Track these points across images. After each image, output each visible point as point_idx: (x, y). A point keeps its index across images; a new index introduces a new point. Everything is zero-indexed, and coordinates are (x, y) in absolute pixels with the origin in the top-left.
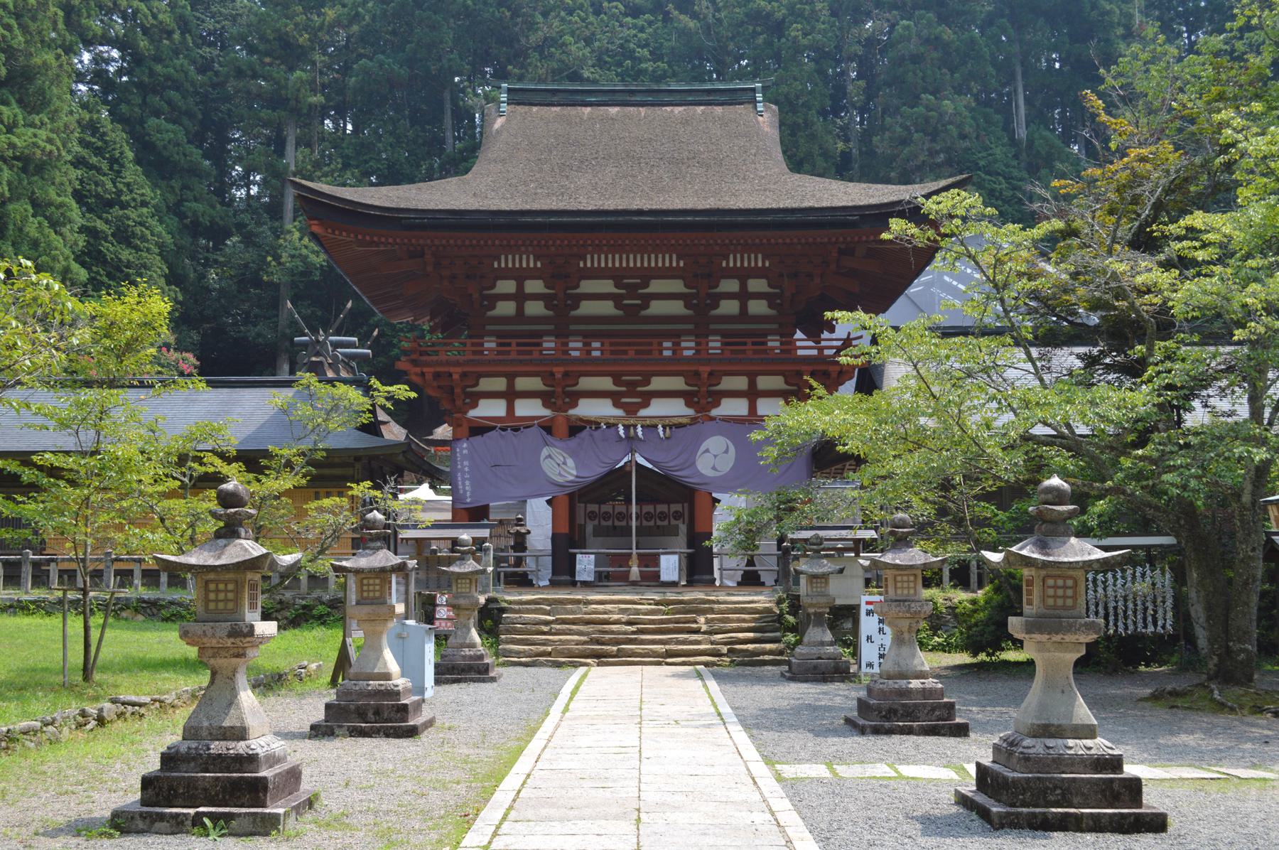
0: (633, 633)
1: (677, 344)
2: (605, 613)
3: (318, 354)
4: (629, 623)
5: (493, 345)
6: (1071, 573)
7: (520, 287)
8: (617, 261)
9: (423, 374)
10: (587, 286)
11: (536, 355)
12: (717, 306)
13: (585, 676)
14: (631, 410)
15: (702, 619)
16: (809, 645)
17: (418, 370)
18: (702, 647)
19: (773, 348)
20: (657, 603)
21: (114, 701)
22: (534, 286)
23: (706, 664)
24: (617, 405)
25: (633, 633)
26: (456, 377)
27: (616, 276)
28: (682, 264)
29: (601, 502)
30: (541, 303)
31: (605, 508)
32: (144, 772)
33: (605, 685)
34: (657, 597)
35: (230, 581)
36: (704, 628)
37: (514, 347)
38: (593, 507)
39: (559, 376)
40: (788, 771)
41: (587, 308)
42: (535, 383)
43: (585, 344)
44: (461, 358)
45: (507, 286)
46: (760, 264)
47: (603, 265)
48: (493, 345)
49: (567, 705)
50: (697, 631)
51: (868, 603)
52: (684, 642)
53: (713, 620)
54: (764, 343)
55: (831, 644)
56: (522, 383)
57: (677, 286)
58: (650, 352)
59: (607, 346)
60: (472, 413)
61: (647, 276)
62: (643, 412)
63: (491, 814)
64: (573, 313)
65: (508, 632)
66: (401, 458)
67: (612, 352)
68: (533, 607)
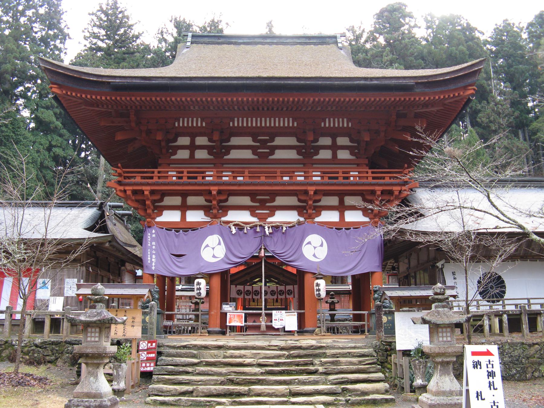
0: (262, 374)
2: (240, 357)
4: (260, 365)
8: (253, 122)
9: (125, 191)
10: (235, 141)
11: (200, 179)
12: (317, 154)
14: (263, 218)
15: (317, 361)
16: (438, 393)
17: (122, 188)
20: (282, 349)
22: (201, 141)
24: (253, 214)
25: (262, 374)
26: (146, 193)
27: (253, 133)
28: (295, 125)
29: (244, 284)
30: (206, 151)
31: (248, 288)
34: (282, 344)
36: (321, 369)
38: (240, 287)
39: (214, 193)
41: (234, 154)
42: (200, 200)
46: (345, 125)
47: (245, 125)
51: (474, 354)
52: (304, 383)
53: (326, 363)
56: (191, 200)
57: (292, 141)
60: (158, 219)
62: (270, 220)
66: (107, 245)
68: (183, 351)
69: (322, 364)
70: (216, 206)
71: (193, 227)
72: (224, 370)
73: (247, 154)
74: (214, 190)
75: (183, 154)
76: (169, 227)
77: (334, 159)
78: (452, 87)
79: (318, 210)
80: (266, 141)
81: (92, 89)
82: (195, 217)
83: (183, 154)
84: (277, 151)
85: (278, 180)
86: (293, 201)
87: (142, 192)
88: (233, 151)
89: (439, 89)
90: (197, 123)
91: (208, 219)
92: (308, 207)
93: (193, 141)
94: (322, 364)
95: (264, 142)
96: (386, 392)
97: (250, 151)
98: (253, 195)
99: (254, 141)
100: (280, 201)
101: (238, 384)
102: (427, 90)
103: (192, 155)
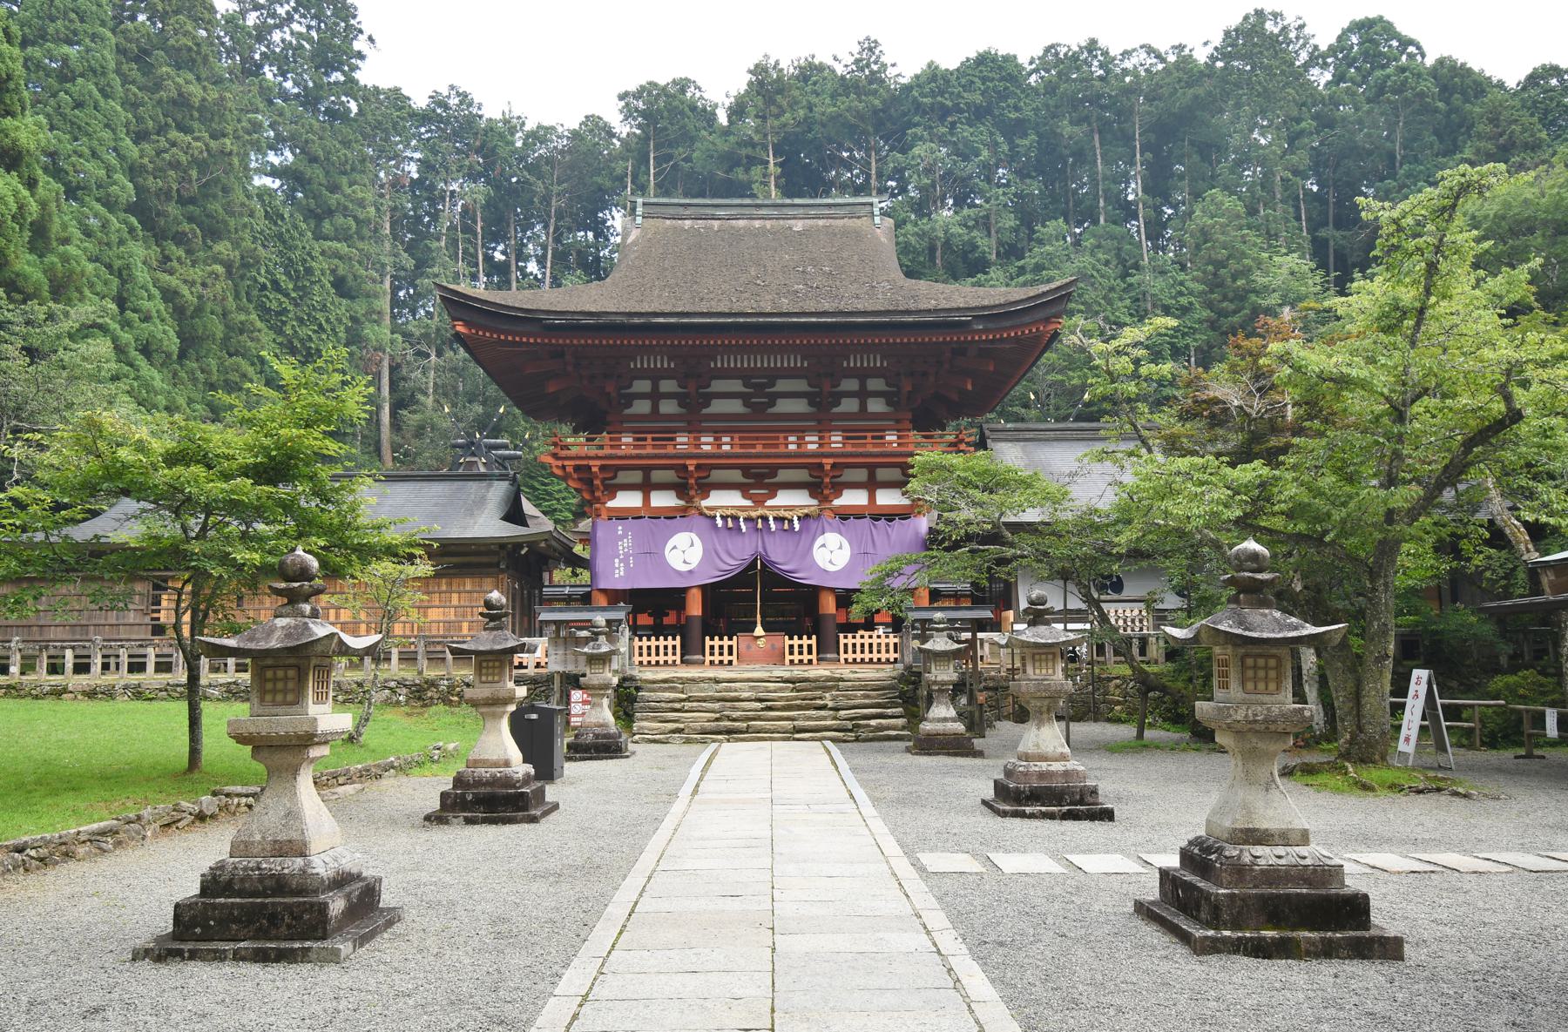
1: (801, 438)
3: (473, 454)
4: (761, 700)
5: (630, 440)
6: (1274, 651)
7: (655, 386)
9: (564, 467)
10: (718, 386)
13: (714, 754)
17: (560, 463)
18: (829, 723)
19: (891, 443)
21: (215, 794)
22: (668, 386)
23: (833, 740)
24: (746, 496)
27: (744, 376)
32: (179, 898)
33: (740, 760)
34: (787, 675)
35: (290, 666)
37: (649, 441)
39: (691, 468)
40: (936, 861)
41: (718, 407)
43: (716, 439)
44: (601, 453)
45: (643, 386)
48: (630, 440)
49: (697, 786)
50: (823, 707)
52: (809, 718)
54: (882, 437)
55: (953, 720)
56: (657, 476)
57: (801, 385)
58: (776, 446)
59: (737, 441)
60: (610, 504)
61: (774, 375)
63: (602, 936)
64: (705, 411)
65: (643, 710)
67: (742, 446)
70: (692, 483)
72: (717, 706)
73: (735, 406)
74: (691, 464)
75: (642, 407)
77: (863, 412)
78: (1027, 319)
79: (838, 489)
80: (763, 476)
81: (520, 329)
82: (663, 500)
83: (642, 407)
84: (780, 401)
85: (782, 449)
86: (802, 475)
87: (590, 467)
88: (715, 402)
89: (1008, 324)
90: (663, 363)
92: (822, 483)
95: (759, 397)
96: (903, 728)
98: (746, 470)
100: (783, 475)
101: (734, 720)
102: (990, 325)
103: (655, 407)
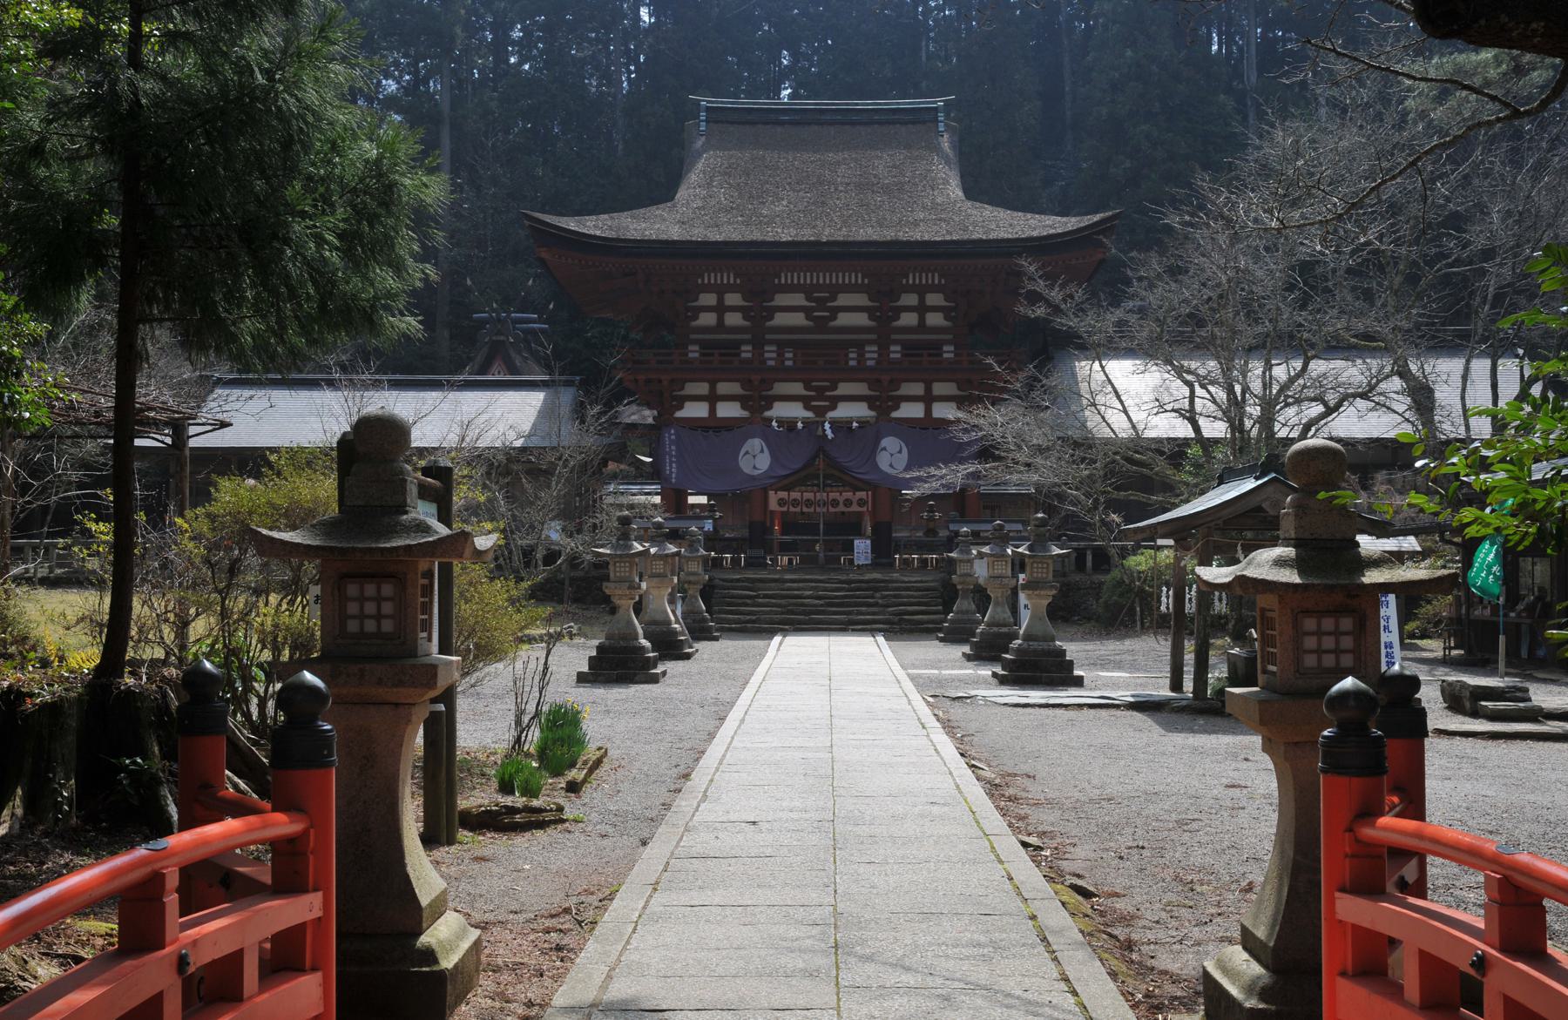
10: (782, 300)
14: (820, 412)
24: (807, 408)
38: (783, 494)
57: (861, 300)
60: (679, 414)
62: (831, 414)
69: (883, 597)
71: (729, 425)
72: (783, 602)
76: (693, 424)
84: (841, 315)
91: (745, 414)
93: (721, 300)
94: (883, 597)
97: (802, 315)
99: (808, 299)
